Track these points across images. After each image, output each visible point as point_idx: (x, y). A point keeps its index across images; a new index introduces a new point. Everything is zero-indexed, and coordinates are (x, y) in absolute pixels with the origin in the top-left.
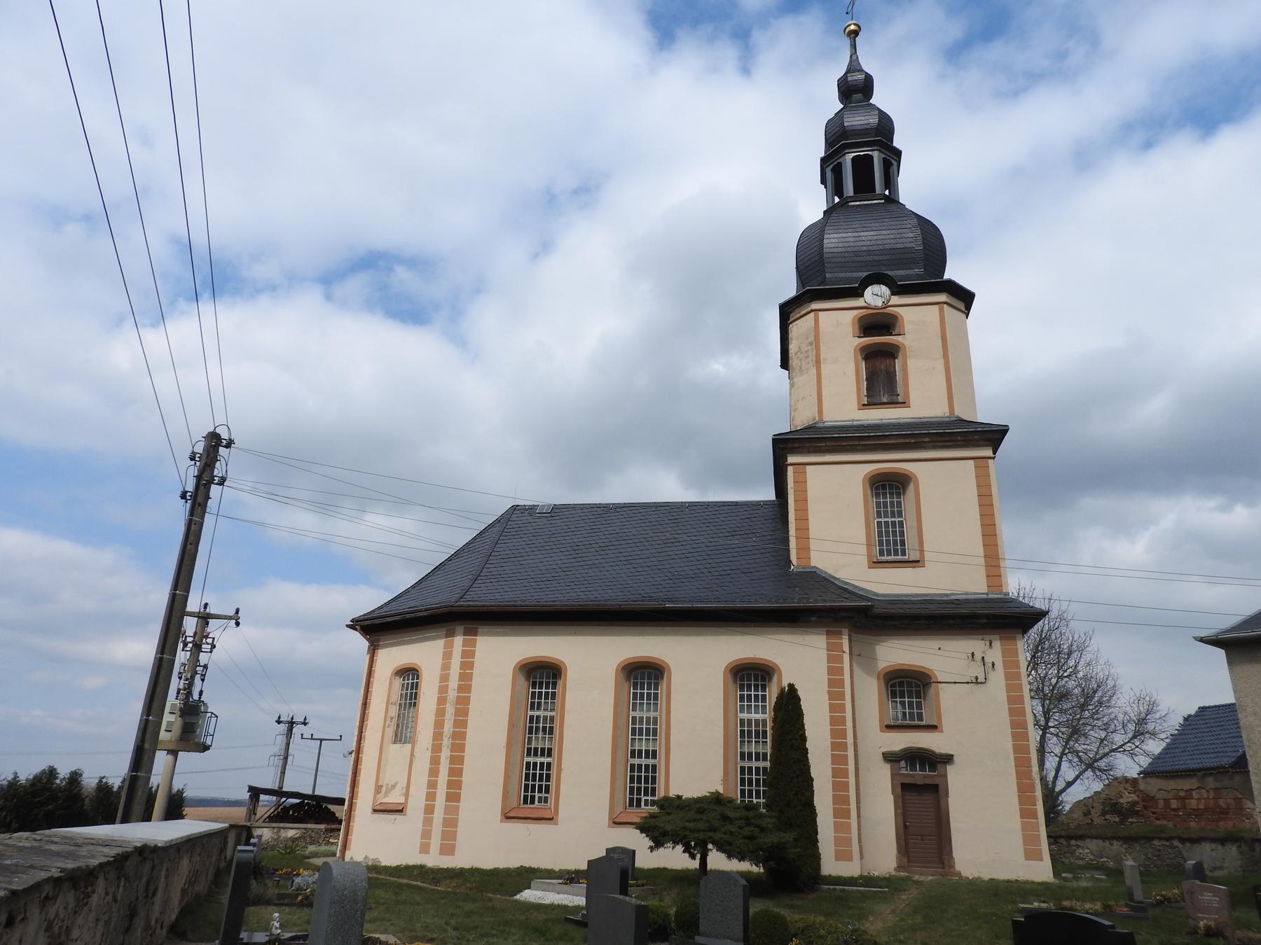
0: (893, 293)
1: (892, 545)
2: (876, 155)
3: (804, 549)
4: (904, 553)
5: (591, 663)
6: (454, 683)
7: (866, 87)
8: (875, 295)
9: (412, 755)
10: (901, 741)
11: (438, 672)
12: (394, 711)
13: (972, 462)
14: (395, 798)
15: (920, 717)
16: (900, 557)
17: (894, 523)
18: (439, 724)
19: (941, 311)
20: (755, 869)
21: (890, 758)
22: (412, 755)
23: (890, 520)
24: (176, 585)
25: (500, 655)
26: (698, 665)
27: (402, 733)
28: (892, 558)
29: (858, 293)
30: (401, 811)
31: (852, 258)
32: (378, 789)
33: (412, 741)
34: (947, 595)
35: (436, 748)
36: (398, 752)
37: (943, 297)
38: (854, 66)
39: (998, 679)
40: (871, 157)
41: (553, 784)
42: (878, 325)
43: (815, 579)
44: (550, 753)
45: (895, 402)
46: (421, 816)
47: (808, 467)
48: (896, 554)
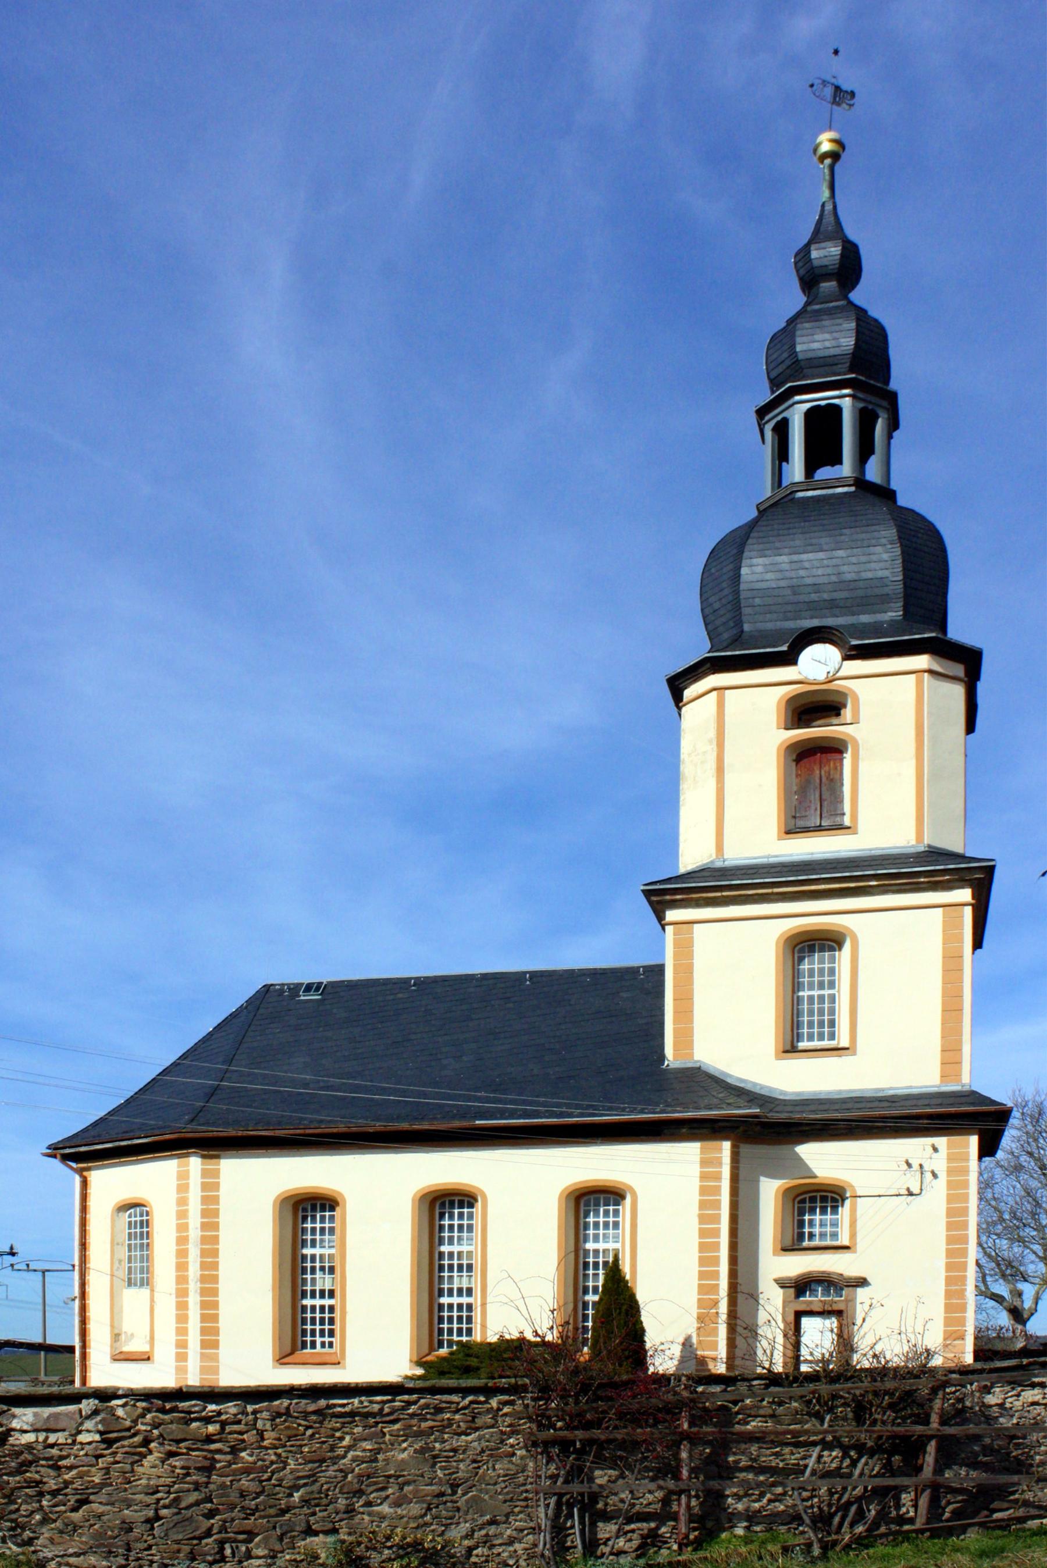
0: (846, 658)
1: (800, 1029)
2: (847, 404)
3: (685, 1038)
4: (832, 1036)
5: (378, 1190)
6: (195, 1221)
7: (850, 268)
8: (819, 662)
9: (152, 1300)
10: (798, 1265)
11: (173, 1208)
12: (123, 1253)
13: (941, 909)
14: (136, 1345)
15: (834, 1235)
16: (826, 1043)
17: (821, 998)
18: (182, 1267)
19: (919, 684)
20: (714, 1429)
21: (782, 1283)
22: (152, 1300)
23: (816, 993)
24: (737, 1229)
25: (256, 1184)
26: (521, 1189)
27: (139, 1274)
28: (816, 1044)
29: (789, 659)
30: (148, 1359)
31: (796, 598)
32: (116, 1337)
33: (146, 1282)
34: (883, 1090)
35: (182, 1293)
36: (134, 1299)
37: (922, 661)
38: (829, 227)
39: (937, 1193)
40: (837, 410)
41: (337, 1327)
42: (814, 707)
43: (700, 1080)
44: (332, 1294)
45: (834, 824)
46: (173, 1363)
47: (695, 926)
48: (821, 1037)
